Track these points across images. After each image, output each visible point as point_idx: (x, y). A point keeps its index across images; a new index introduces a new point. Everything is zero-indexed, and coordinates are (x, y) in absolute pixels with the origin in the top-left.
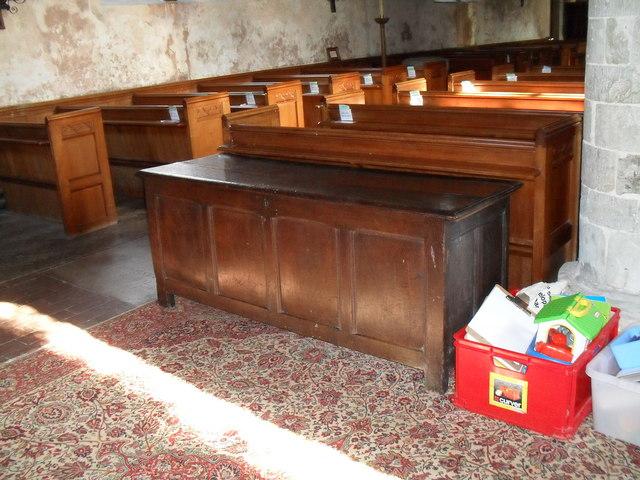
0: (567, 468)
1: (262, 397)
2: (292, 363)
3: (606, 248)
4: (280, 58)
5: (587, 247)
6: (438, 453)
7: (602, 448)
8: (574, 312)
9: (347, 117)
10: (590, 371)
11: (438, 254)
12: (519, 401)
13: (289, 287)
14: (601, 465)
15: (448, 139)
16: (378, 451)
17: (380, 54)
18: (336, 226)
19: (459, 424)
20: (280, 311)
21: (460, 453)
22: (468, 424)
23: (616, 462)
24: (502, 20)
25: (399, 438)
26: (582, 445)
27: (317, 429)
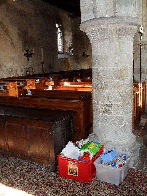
0: (89, 191)
1: (2, 177)
2: (12, 166)
3: (100, 129)
4: (12, 74)
5: (95, 129)
6: (53, 190)
7: (99, 184)
8: (90, 147)
9: (29, 93)
10: (95, 163)
11: (52, 133)
12: (76, 173)
13: (11, 144)
14: (98, 189)
15: (56, 100)
16: (36, 191)
17: (42, 73)
18: (23, 126)
19: (60, 181)
20: (8, 151)
21: (59, 189)
22: (62, 181)
23: (102, 188)
24: (78, 62)
25: (42, 186)
26: (94, 184)
27: (18, 186)
